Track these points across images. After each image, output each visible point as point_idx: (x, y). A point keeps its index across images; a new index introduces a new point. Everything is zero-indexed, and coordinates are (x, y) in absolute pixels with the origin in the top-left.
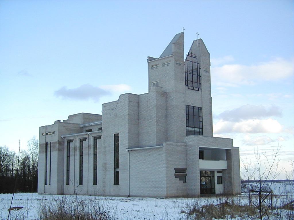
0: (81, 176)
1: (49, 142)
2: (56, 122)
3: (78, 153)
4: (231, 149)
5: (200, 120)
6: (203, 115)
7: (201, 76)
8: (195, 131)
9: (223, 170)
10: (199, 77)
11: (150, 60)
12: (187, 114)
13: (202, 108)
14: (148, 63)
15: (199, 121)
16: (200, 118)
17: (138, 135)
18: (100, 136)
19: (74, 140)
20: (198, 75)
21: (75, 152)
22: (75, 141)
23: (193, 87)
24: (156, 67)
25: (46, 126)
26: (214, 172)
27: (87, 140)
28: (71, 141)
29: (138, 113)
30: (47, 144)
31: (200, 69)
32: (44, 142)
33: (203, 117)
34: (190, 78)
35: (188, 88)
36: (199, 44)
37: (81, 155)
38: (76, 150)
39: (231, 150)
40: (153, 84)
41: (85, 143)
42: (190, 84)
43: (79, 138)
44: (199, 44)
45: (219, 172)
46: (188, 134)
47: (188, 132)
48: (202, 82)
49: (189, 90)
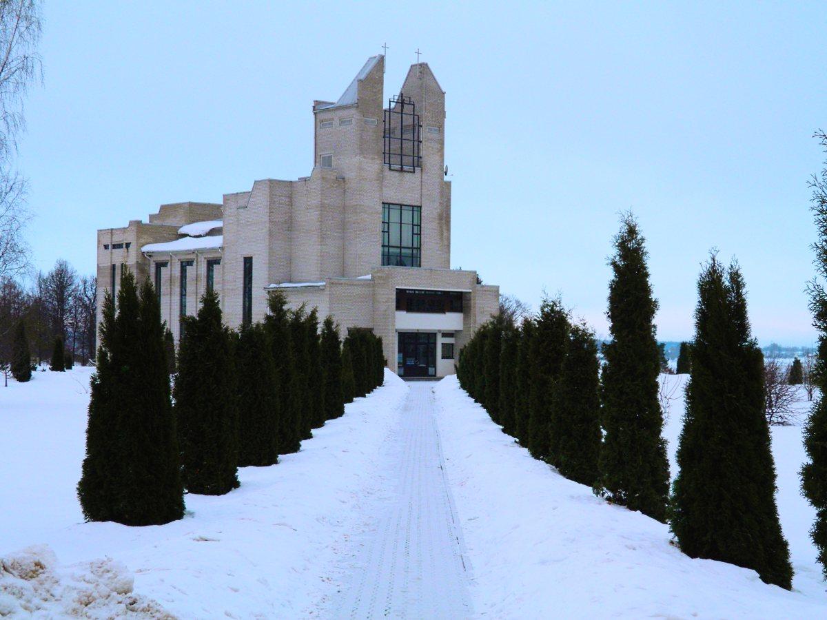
0: (210, 286)
1: (118, 265)
2: (131, 223)
3: (177, 290)
4: (471, 291)
5: (415, 232)
6: (422, 223)
7: (421, 142)
9: (456, 331)
10: (416, 143)
11: (320, 108)
12: (386, 220)
13: (421, 207)
14: (315, 114)
15: (413, 234)
16: (415, 228)
17: (290, 260)
19: (195, 261)
20: (416, 138)
22: (197, 263)
23: (401, 165)
24: (329, 124)
25: (112, 230)
26: (435, 334)
27: (195, 264)
28: (164, 264)
29: (291, 217)
30: (113, 267)
33: (422, 225)
34: (395, 146)
35: (390, 169)
36: (421, 72)
37: (183, 295)
39: (470, 292)
42: (395, 160)
44: (421, 72)
45: (445, 335)
49: (392, 173)
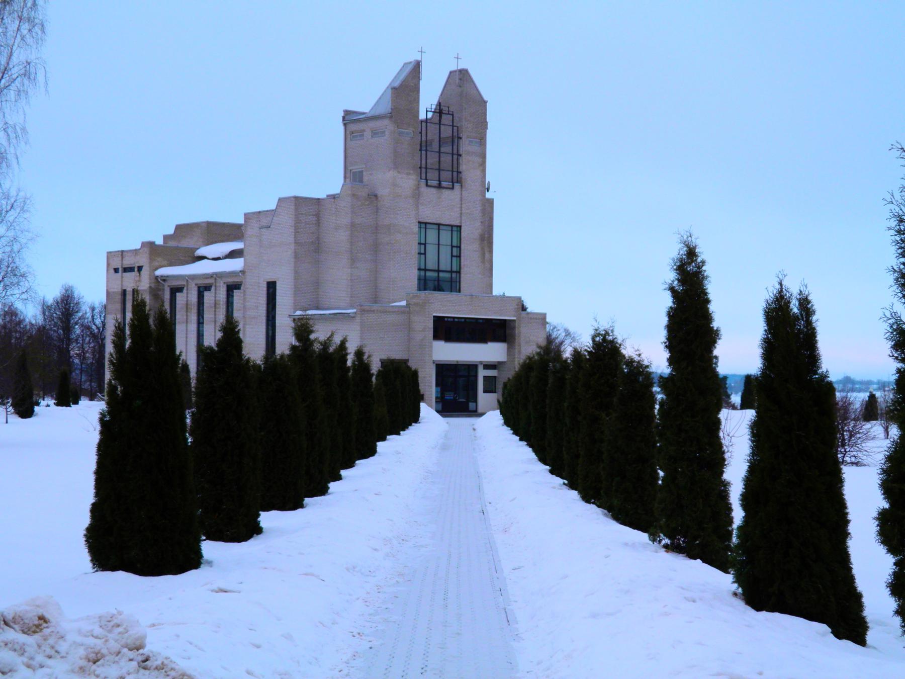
3: (194, 317)
4: (515, 318)
8: (440, 279)
9: (499, 362)
10: (455, 157)
11: (350, 119)
17: (317, 284)
18: (209, 283)
19: (185, 288)
20: (455, 152)
21: (189, 314)
27: (213, 289)
28: (180, 289)
30: (124, 293)
31: (461, 138)
32: (118, 289)
33: (463, 247)
38: (189, 310)
39: (514, 320)
40: (353, 172)
41: (208, 297)
42: (433, 175)
43: (224, 283)
45: (487, 366)
46: (422, 287)
47: (422, 282)
48: (463, 168)
